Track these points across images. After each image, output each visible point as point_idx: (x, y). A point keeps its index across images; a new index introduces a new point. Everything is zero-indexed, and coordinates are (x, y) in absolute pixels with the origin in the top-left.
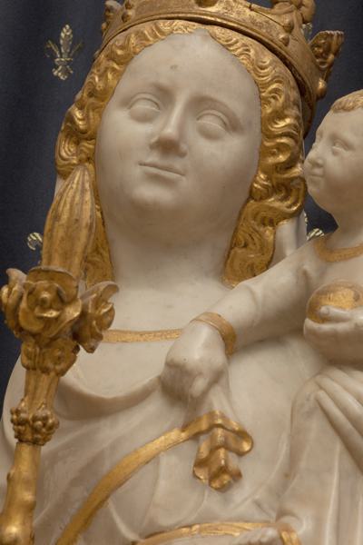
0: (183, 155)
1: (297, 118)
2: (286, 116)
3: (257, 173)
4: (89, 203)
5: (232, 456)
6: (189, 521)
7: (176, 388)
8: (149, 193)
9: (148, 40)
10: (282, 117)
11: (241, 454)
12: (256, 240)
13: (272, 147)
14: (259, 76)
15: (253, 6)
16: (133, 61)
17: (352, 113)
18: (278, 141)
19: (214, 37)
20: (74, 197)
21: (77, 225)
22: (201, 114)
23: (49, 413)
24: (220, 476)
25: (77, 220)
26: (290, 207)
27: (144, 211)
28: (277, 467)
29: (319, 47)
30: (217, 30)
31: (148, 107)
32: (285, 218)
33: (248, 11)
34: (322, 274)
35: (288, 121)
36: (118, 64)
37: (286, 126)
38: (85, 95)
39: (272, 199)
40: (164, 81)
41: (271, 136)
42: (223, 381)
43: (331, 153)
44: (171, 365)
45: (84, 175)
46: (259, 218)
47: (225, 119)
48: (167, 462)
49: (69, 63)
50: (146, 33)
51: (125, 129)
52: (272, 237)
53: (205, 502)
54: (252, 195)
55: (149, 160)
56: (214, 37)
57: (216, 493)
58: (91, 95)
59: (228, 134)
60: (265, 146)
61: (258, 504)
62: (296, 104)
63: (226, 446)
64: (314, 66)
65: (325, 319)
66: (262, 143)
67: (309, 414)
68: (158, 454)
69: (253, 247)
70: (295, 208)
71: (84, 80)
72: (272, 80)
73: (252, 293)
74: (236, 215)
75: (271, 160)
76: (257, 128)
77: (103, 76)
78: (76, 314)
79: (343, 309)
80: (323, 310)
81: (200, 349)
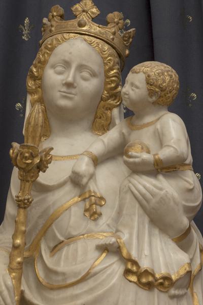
0: (75, 88)
1: (118, 69)
4: (41, 117)
5: (98, 207)
6: (83, 233)
7: (76, 180)
8: (63, 103)
9: (60, 42)
10: (113, 70)
11: (101, 206)
13: (109, 81)
17: (139, 74)
19: (85, 40)
20: (35, 115)
23: (29, 197)
24: (94, 215)
26: (117, 103)
27: (62, 110)
28: (115, 209)
29: (126, 37)
30: (86, 37)
33: (98, 28)
34: (130, 134)
35: (115, 71)
40: (67, 59)
42: (94, 178)
44: (74, 173)
46: (105, 108)
48: (74, 209)
49: (28, 33)
51: (53, 77)
53: (89, 226)
54: (102, 99)
55: (62, 90)
56: (85, 40)
57: (93, 222)
58: (39, 62)
61: (108, 225)
62: (118, 63)
63: (95, 203)
64: (124, 46)
65: (130, 157)
67: (126, 192)
68: (70, 207)
70: (119, 103)
71: (35, 57)
73: (103, 142)
75: (109, 86)
78: (38, 161)
79: (137, 153)
80: (130, 153)
81: (84, 166)
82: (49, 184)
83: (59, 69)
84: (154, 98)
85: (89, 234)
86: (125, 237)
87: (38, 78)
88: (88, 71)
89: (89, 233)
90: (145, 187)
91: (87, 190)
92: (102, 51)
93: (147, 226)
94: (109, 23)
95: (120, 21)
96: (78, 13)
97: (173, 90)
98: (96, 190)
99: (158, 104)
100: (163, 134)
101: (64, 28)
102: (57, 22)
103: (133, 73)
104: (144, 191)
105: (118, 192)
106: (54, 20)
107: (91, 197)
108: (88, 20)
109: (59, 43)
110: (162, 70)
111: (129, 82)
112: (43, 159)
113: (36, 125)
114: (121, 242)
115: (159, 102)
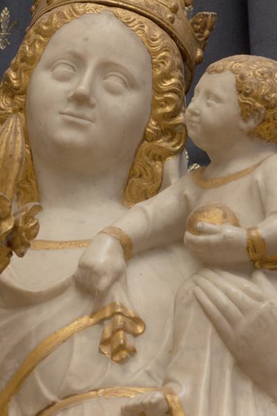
0: (92, 106)
1: (180, 78)
2: (172, 77)
3: (149, 120)
4: (20, 142)
5: (129, 337)
6: (96, 386)
7: (86, 284)
8: (67, 135)
9: (66, 18)
10: (169, 78)
11: (136, 335)
13: (161, 101)
14: (152, 46)
16: (55, 34)
17: (222, 74)
18: (166, 96)
19: (117, 16)
20: (9, 138)
24: (120, 352)
25: (11, 156)
26: (174, 146)
27: (63, 150)
30: (119, 11)
32: (170, 155)
34: (199, 197)
35: (173, 80)
36: (43, 37)
38: (18, 60)
39: (161, 140)
40: (78, 50)
44: (83, 267)
47: (124, 77)
48: (79, 341)
49: (7, 36)
50: (65, 13)
52: (161, 170)
54: (145, 137)
56: (117, 16)
57: (117, 365)
58: (22, 60)
60: (156, 100)
61: (149, 374)
62: (179, 67)
63: (124, 329)
65: (200, 232)
66: (153, 97)
68: (72, 335)
69: (146, 177)
70: (178, 147)
72: (161, 49)
73: (145, 212)
75: (160, 111)
76: (149, 86)
77: (32, 46)
78: (10, 227)
79: (214, 224)
80: (199, 225)
81: (104, 255)
82: (33, 291)
83: (62, 69)
84: (252, 123)
85: (108, 390)
86: (182, 392)
88: (120, 75)
89: (109, 386)
90: (227, 293)
91: (108, 302)
93: (228, 373)
98: (127, 304)
99: (259, 136)
103: (210, 73)
104: (224, 300)
105: (172, 306)
107: (116, 316)
110: (269, 68)
111: (202, 91)
112: (20, 225)
114: (173, 401)
115: (261, 133)
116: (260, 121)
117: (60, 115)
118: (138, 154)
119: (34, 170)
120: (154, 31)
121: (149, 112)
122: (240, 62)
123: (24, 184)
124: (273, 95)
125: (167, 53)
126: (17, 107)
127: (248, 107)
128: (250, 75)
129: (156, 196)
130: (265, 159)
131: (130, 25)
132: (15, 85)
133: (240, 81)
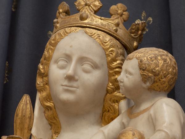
0: (77, 80)
2: (117, 60)
3: (108, 83)
8: (65, 96)
9: (62, 36)
10: (116, 61)
12: (112, 109)
13: (113, 73)
14: (105, 46)
15: (102, 18)
16: (58, 45)
17: (132, 60)
18: (115, 70)
19: (86, 33)
21: (24, 118)
22: (83, 63)
25: (24, 116)
27: (65, 103)
29: (133, 29)
30: (87, 30)
31: (63, 63)
32: (122, 99)
33: (100, 20)
34: (128, 123)
35: (118, 62)
36: (53, 47)
37: (116, 64)
38: (43, 59)
39: (116, 92)
40: (68, 52)
41: (112, 69)
43: (125, 77)
45: (27, 98)
47: (92, 65)
50: (62, 33)
51: (56, 72)
52: (118, 107)
54: (108, 92)
56: (86, 33)
58: (45, 59)
59: (94, 70)
60: (110, 73)
66: (109, 71)
69: (111, 112)
72: (110, 47)
73: (104, 133)
74: (103, 100)
77: (48, 51)
84: (148, 84)
87: (45, 75)
92: (103, 43)
94: (112, 15)
95: (124, 13)
96: (80, 7)
97: (168, 74)
99: (154, 90)
100: (156, 119)
101: (67, 23)
102: (62, 18)
103: (127, 60)
106: (60, 17)
108: (90, 13)
109: (61, 37)
110: (155, 54)
113: (24, 116)
116: (152, 82)
117: (61, 86)
118: (105, 101)
119: (57, 113)
120: (105, 38)
121: (107, 79)
122: (141, 53)
123: (53, 120)
124: (157, 69)
125: (114, 48)
126: (44, 83)
127: (145, 76)
128: (145, 60)
129: (107, 125)
130: (154, 103)
131: (93, 36)
132: (42, 72)
133: (140, 63)
